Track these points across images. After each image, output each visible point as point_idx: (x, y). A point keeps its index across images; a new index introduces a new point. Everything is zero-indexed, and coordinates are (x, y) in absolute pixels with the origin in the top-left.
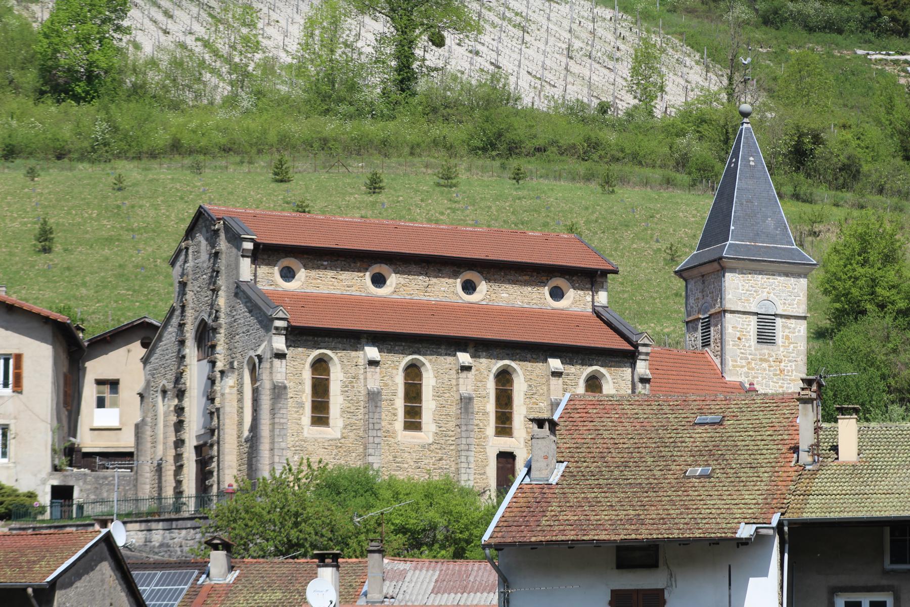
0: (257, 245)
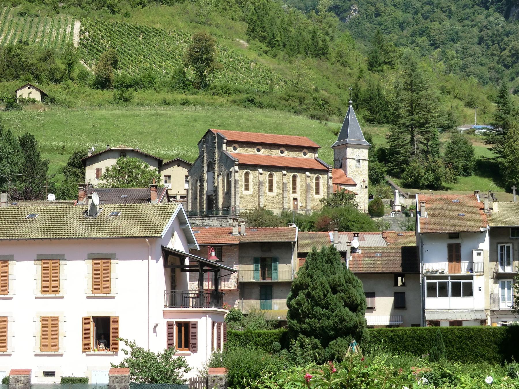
0: (227, 141)
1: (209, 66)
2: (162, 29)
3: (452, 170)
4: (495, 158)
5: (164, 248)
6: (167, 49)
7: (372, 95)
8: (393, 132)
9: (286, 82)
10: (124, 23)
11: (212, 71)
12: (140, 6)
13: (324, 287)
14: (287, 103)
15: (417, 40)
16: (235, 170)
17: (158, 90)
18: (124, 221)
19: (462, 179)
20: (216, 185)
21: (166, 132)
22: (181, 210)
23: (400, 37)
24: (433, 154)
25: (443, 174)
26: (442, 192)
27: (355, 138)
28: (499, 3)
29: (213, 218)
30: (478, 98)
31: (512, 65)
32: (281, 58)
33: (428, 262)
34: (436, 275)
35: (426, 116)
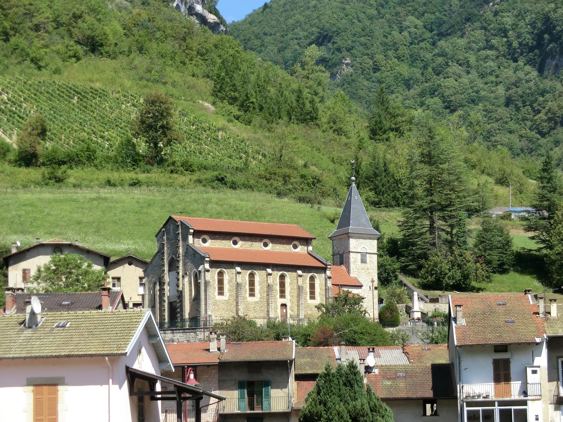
0: (195, 231)
1: (166, 136)
2: (103, 88)
3: (484, 265)
4: (539, 250)
5: (130, 370)
6: (109, 114)
7: (377, 171)
8: (407, 217)
9: (264, 156)
10: (54, 82)
11: (169, 143)
12: (74, 60)
13: (342, 417)
14: (268, 183)
15: (427, 102)
16: (205, 268)
17: (100, 168)
18: (75, 334)
19: (497, 277)
20: (180, 289)
21: (112, 221)
22: (150, 318)
23: (405, 97)
24: (459, 246)
25: (472, 271)
26: (472, 293)
27: (359, 225)
28: (531, 54)
29: (177, 331)
30: (512, 173)
31: (549, 132)
32: (257, 125)
33: (468, 383)
34: (479, 400)
35: (449, 196)
